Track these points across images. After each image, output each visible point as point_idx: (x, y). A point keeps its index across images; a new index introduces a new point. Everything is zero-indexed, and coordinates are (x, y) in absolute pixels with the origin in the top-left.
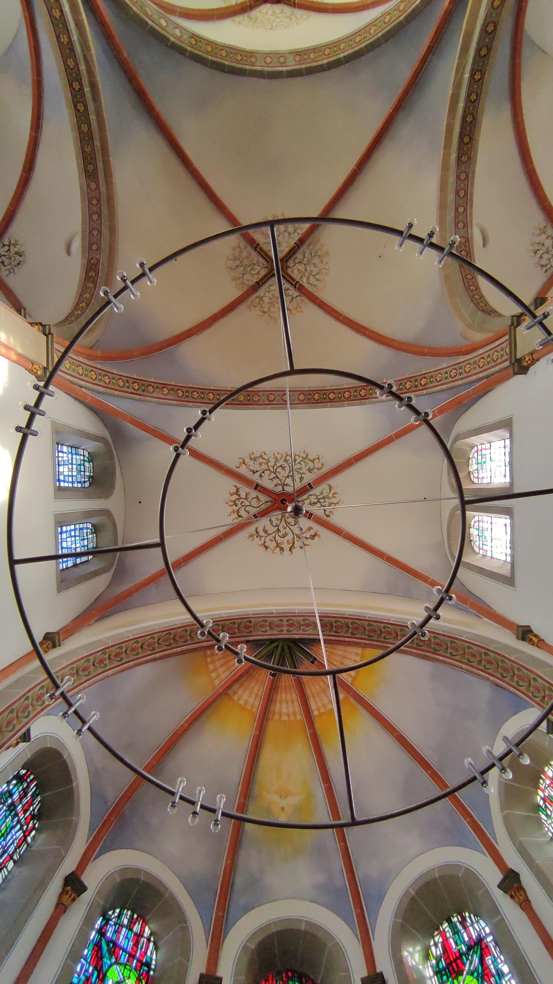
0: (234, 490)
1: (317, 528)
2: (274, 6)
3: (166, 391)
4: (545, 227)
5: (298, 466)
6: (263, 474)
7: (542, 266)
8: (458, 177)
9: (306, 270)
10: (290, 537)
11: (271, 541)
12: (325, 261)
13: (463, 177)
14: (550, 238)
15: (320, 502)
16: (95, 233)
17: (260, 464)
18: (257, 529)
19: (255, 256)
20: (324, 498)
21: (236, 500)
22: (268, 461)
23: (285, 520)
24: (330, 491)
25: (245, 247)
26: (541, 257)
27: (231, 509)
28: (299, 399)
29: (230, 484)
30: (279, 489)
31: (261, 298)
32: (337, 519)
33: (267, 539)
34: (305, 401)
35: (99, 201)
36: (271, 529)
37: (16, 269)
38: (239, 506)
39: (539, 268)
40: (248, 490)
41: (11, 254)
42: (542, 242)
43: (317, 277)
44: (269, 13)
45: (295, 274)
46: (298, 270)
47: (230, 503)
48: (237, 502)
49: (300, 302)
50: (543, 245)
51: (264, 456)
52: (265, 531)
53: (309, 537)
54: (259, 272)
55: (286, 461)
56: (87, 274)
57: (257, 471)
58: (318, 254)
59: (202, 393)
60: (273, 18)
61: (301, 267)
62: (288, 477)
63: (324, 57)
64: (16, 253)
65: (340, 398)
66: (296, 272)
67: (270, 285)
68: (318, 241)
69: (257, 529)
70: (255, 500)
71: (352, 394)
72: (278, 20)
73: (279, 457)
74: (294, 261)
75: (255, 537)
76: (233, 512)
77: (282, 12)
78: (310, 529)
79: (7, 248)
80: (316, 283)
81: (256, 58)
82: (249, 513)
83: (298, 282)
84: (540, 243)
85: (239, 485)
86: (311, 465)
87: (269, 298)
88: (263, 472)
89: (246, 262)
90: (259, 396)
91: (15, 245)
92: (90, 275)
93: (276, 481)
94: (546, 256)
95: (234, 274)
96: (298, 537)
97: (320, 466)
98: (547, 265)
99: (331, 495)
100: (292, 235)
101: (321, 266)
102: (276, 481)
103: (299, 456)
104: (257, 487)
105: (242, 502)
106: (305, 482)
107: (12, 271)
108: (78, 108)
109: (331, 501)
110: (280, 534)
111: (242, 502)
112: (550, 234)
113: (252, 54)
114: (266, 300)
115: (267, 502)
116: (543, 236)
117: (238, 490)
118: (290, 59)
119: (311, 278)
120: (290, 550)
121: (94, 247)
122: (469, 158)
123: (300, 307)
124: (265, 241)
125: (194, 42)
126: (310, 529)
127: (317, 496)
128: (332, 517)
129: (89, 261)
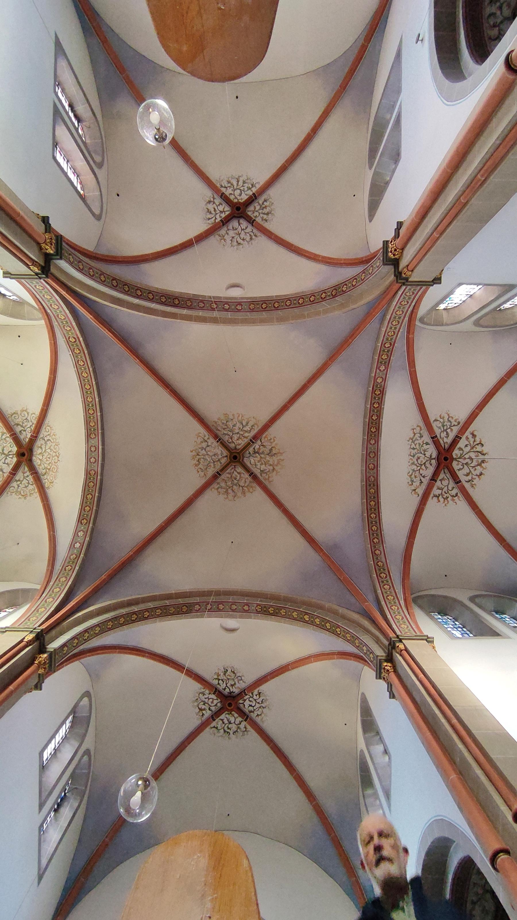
0: (435, 499)
1: (468, 433)
2: (34, 453)
3: (377, 552)
4: (219, 236)
5: (417, 446)
6: (423, 475)
7: (251, 239)
8: (202, 308)
9: (238, 433)
10: (473, 455)
11: (476, 469)
12: (231, 417)
13: (201, 305)
14: (228, 232)
15: (447, 429)
16: (234, 607)
17: (416, 477)
18: (466, 481)
19: (225, 476)
20: (443, 426)
21: (444, 498)
22: (414, 470)
23: (459, 458)
24: (438, 420)
25: (218, 483)
26: (243, 240)
27: (451, 502)
28: (374, 444)
29: (431, 502)
30: (434, 462)
31: (262, 471)
32: (462, 416)
33: (474, 473)
34: (376, 440)
35: (222, 603)
36: (466, 470)
37: (238, 675)
38: (448, 495)
39: (253, 241)
40: (435, 488)
41: (225, 678)
42: (231, 239)
43: (244, 424)
44: (41, 458)
45: (242, 443)
46: (238, 440)
47: (446, 502)
48: (445, 497)
49: (266, 439)
50: (233, 237)
51: (410, 474)
52: (467, 475)
53: (473, 439)
54: (238, 473)
55: (414, 456)
56: (271, 614)
57: (421, 480)
58: (225, 422)
59: (372, 523)
60: (46, 455)
61: (235, 437)
62: (425, 455)
63: (95, 414)
64: (225, 674)
65: (378, 411)
66: (240, 442)
67: (250, 463)
68: (216, 423)
69: (466, 481)
70: (443, 482)
71: (376, 401)
72: (49, 451)
73: (411, 462)
74: (230, 443)
75: (473, 483)
76: (453, 500)
77: (41, 447)
78: (467, 438)
79: (220, 682)
80: (250, 425)
81: (91, 470)
82: (454, 488)
83: (251, 440)
84: (231, 240)
85: (432, 495)
86: (418, 435)
87: (261, 465)
88: (421, 475)
89: (229, 483)
90: (370, 477)
91: (219, 675)
92: (272, 612)
93: (428, 465)
94: (243, 235)
95: (239, 494)
96: (472, 448)
97: (419, 428)
98: (250, 235)
99: (442, 420)
100: (209, 444)
101: (235, 420)
102: (428, 465)
103: (411, 445)
104: (434, 479)
105: (445, 492)
106: (430, 441)
107: (240, 678)
108: (146, 616)
109: (446, 420)
110: (470, 462)
111: (445, 492)
112: (225, 232)
113: (88, 473)
114: (263, 467)
115: (444, 472)
116: (226, 237)
117: (435, 496)
118: (93, 442)
119: (245, 429)
120: (483, 454)
121: (246, 608)
122: (189, 299)
123: (271, 439)
124: (212, 466)
125: (85, 521)
126: (467, 438)
127: (441, 432)
128: (460, 420)
129: (258, 612)
